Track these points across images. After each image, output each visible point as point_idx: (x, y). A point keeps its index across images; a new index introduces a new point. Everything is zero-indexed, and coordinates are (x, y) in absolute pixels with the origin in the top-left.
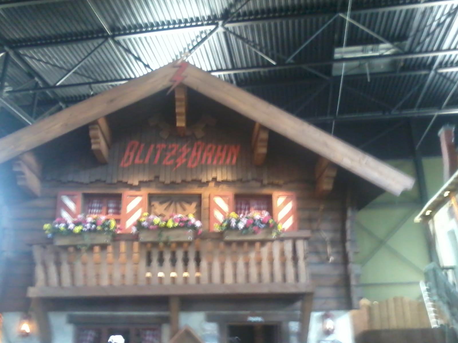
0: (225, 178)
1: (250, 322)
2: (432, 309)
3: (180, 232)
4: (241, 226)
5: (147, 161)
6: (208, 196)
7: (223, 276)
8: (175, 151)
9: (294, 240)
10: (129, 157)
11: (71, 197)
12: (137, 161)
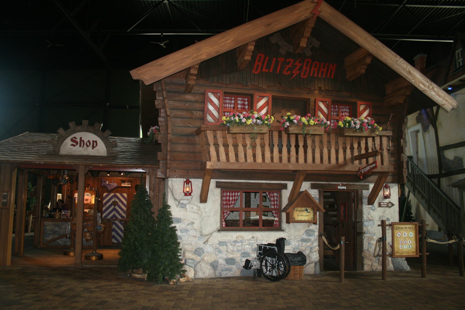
0: (327, 88)
1: (340, 189)
2: (31, 185)
3: (316, 128)
4: (358, 126)
5: (271, 71)
6: (313, 101)
7: (337, 159)
8: (290, 64)
9: (381, 137)
10: (258, 65)
11: (215, 94)
12: (264, 70)
